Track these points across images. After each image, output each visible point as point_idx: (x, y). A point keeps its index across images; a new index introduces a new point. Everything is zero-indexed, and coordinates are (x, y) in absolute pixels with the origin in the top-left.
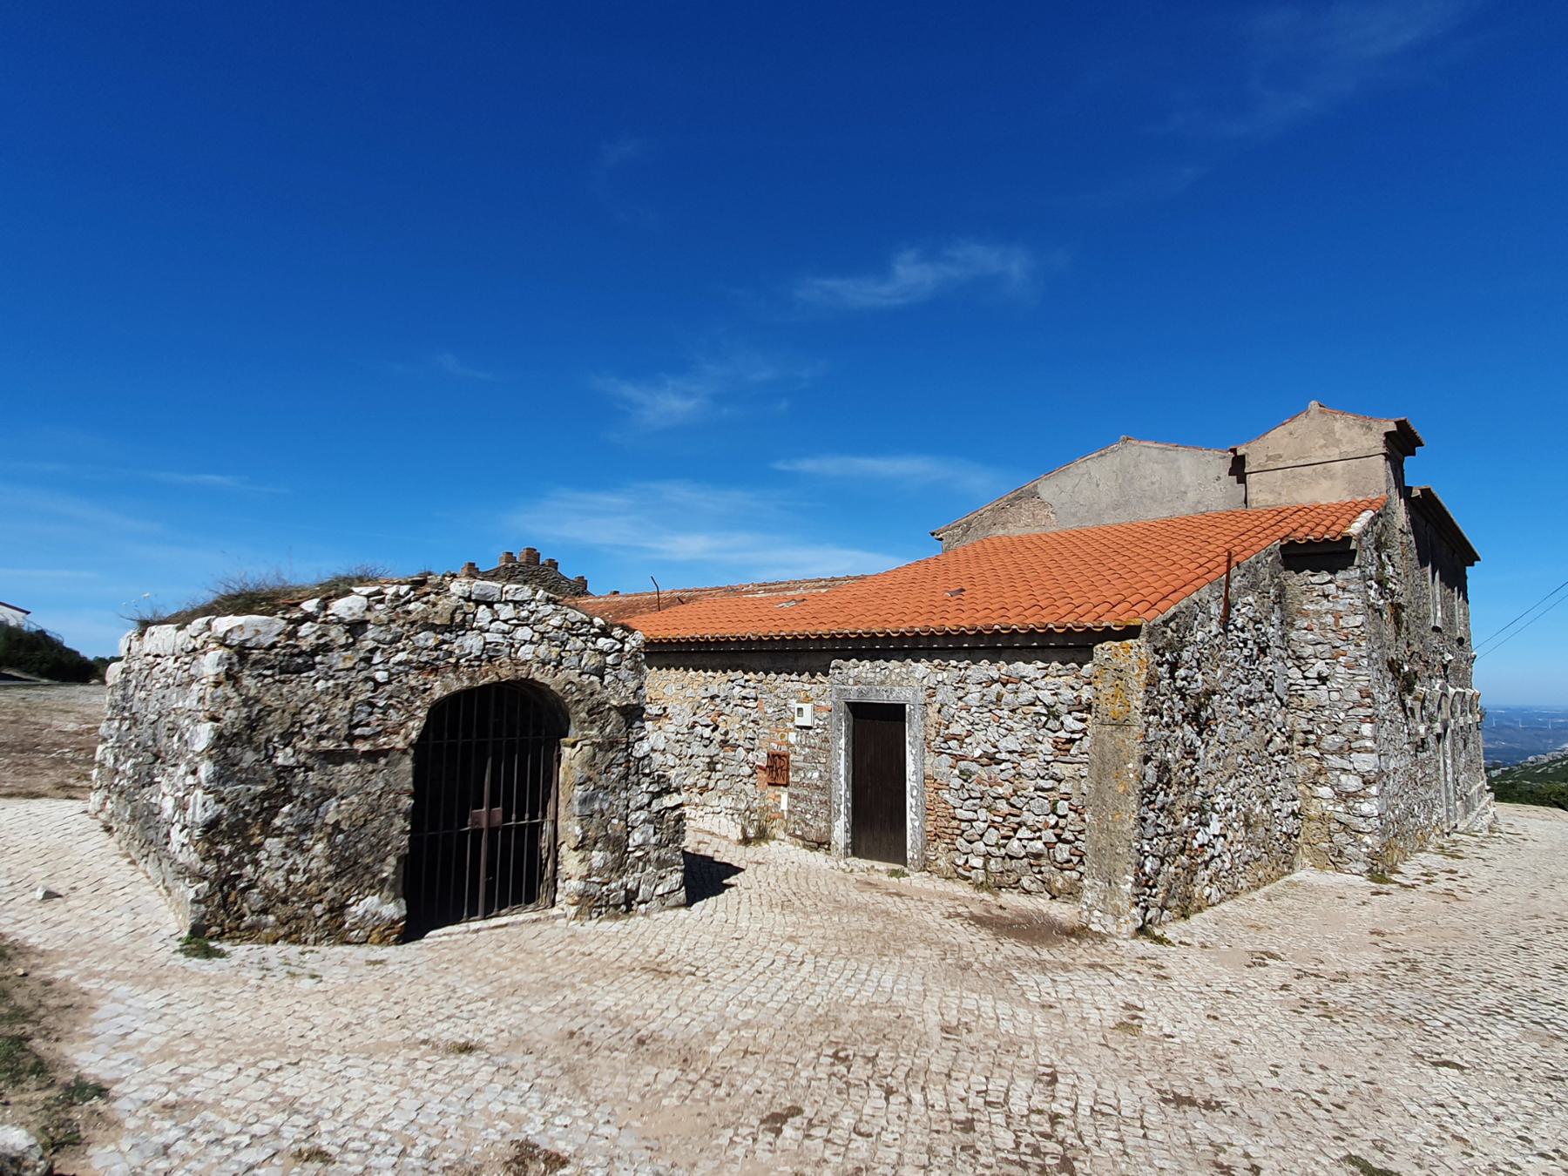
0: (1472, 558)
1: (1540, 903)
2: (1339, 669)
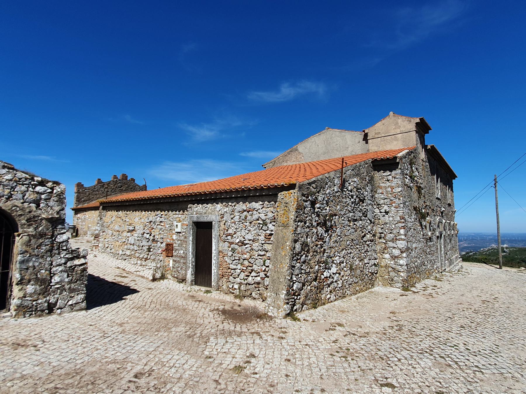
0: (454, 177)
1: (464, 298)
2: (393, 208)
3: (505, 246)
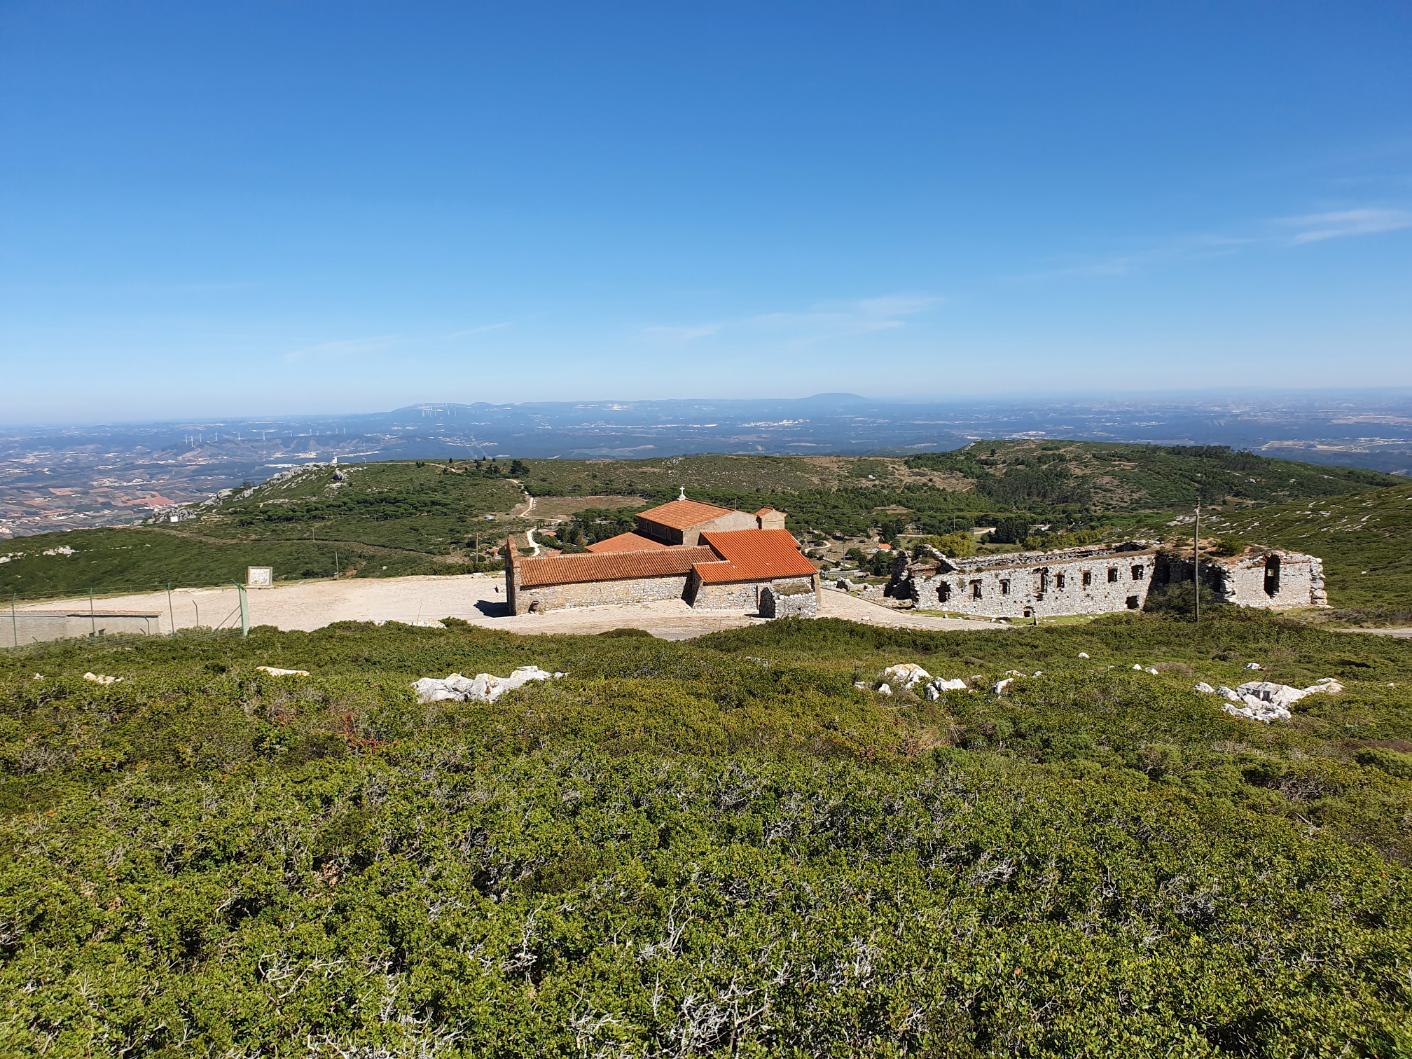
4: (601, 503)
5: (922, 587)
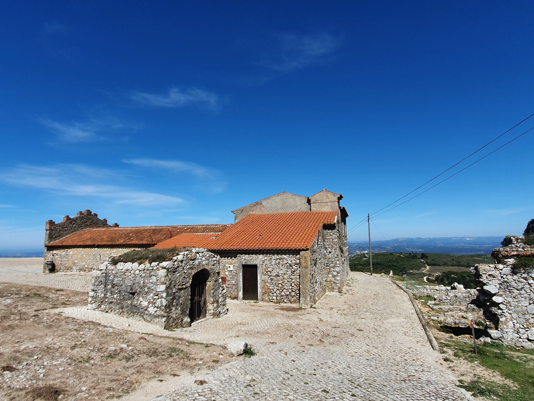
2: (333, 250)
3: (366, 252)
4: (455, 269)
5: (505, 286)
